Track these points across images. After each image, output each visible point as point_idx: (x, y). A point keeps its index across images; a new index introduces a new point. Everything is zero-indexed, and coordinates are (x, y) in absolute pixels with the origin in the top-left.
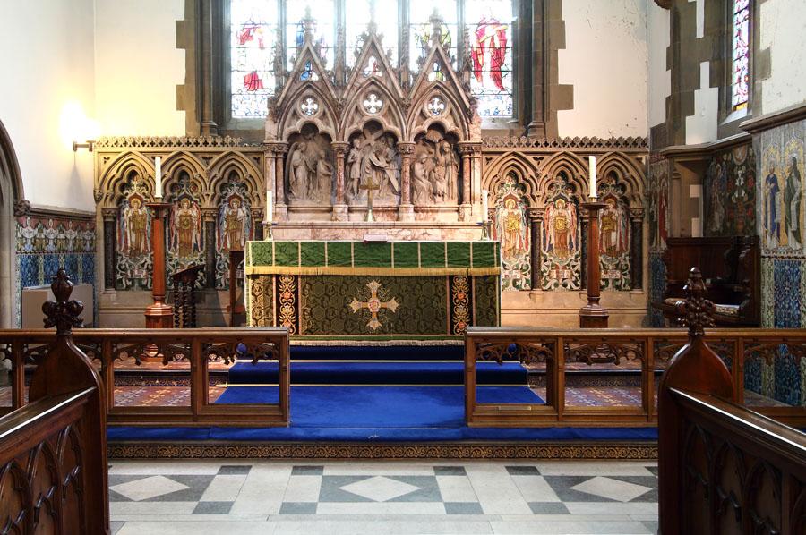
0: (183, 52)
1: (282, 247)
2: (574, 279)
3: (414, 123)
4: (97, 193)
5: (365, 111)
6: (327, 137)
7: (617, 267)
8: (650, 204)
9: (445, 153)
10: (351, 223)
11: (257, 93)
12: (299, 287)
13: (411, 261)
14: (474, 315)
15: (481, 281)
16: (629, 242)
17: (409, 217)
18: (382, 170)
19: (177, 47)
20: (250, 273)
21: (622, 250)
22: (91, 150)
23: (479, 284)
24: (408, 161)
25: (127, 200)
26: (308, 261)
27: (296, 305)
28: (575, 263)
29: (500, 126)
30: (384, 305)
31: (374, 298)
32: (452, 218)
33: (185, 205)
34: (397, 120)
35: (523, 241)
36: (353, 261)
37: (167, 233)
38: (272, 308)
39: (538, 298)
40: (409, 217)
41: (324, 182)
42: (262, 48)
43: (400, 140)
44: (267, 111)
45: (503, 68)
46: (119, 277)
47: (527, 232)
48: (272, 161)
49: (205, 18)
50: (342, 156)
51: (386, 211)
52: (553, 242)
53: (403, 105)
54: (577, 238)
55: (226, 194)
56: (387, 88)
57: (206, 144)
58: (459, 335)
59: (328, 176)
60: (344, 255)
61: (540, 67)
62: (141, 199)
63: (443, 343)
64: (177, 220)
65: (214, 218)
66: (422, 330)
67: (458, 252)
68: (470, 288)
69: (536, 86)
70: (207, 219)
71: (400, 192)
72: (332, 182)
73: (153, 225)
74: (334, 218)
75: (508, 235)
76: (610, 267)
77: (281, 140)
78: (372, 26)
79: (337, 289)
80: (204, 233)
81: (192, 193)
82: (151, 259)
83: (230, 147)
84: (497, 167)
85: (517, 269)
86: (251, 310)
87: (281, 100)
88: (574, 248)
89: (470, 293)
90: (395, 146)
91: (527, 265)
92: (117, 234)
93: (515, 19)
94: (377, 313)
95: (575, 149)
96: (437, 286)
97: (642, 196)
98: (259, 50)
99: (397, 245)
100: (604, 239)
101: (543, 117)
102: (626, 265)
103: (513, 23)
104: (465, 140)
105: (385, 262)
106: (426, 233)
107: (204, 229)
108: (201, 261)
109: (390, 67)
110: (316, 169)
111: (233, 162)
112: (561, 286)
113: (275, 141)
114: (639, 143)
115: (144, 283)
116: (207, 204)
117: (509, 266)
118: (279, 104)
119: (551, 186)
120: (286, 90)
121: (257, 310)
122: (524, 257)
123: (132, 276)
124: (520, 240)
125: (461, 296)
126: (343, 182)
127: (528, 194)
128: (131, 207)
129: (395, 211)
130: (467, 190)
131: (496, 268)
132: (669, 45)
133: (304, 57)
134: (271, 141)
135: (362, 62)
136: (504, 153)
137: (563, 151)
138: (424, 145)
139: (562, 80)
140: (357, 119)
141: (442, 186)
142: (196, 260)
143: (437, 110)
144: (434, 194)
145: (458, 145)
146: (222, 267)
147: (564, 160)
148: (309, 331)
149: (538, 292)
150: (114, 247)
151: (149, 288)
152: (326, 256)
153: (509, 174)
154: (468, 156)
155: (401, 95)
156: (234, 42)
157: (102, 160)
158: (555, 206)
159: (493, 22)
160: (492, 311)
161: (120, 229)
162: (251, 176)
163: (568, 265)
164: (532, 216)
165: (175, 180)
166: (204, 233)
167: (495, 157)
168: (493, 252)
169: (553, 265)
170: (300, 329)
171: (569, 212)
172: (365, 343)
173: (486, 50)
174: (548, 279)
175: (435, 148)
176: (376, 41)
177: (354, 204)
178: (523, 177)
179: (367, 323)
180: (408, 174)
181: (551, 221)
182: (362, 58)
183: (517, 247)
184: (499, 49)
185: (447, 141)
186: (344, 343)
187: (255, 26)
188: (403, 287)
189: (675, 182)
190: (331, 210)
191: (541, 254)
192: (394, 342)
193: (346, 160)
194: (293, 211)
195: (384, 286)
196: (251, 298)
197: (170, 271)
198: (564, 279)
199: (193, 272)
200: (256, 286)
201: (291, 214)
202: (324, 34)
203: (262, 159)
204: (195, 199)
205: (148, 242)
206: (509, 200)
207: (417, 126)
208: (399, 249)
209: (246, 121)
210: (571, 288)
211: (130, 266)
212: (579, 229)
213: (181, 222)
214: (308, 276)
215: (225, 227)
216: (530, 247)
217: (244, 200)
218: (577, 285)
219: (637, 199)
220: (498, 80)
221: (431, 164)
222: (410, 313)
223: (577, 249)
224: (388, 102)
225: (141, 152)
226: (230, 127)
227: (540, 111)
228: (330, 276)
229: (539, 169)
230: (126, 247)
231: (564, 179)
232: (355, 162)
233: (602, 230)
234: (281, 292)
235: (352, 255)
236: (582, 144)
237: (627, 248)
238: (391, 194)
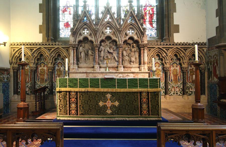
0: (41, 14)
1: (71, 80)
2: (180, 91)
3: (123, 37)
4: (10, 62)
5: (105, 33)
6: (92, 42)
9: (134, 47)
10: (100, 72)
11: (68, 29)
12: (78, 96)
13: (124, 86)
14: (150, 108)
15: (153, 94)
17: (121, 70)
18: (112, 53)
19: (39, 12)
20: (58, 91)
22: (5, 46)
23: (152, 95)
24: (121, 50)
26: (82, 86)
27: (77, 104)
28: (180, 86)
29: (152, 39)
30: (113, 104)
31: (109, 101)
32: (137, 70)
33: (42, 66)
34: (117, 36)
36: (100, 86)
38: (67, 105)
39: (168, 98)
40: (122, 70)
41: (91, 58)
42: (70, 14)
43: (118, 43)
44: (70, 33)
45: (153, 20)
46: (19, 90)
48: (72, 50)
49: (50, 3)
50: (97, 48)
51: (113, 68)
52: (172, 78)
53: (119, 31)
54: (181, 77)
55: (57, 62)
56: (113, 25)
57: (49, 45)
58: (144, 116)
59: (92, 55)
60: (97, 83)
61: (167, 19)
63: (137, 119)
64: (40, 71)
65: (52, 70)
66: (129, 114)
67: (143, 82)
68: (148, 97)
69: (166, 25)
70: (50, 71)
71: (118, 61)
72: (94, 58)
73: (31, 73)
74: (94, 70)
77: (75, 43)
78: (108, 4)
79: (94, 97)
80: (49, 75)
81: (45, 62)
82: (30, 84)
83: (58, 46)
84: (153, 52)
86: (58, 105)
87: (75, 29)
88: (180, 81)
89: (148, 99)
90: (116, 45)
91: (163, 87)
92: (18, 76)
93: (157, 4)
94: (110, 107)
95: (180, 46)
96: (135, 96)
97: (205, 63)
98: (69, 15)
99: (118, 79)
101: (168, 36)
103: (156, 6)
104: (141, 43)
105: (113, 86)
106: (128, 75)
107: (49, 74)
108: (48, 85)
109: (114, 18)
110: (88, 53)
111: (59, 51)
112: (175, 94)
113: (73, 43)
114: (203, 44)
115: (28, 92)
116: (50, 65)
118: (74, 30)
119: (171, 60)
120: (77, 25)
121: (61, 106)
125: (145, 100)
126: (97, 58)
127: (164, 62)
129: (116, 68)
130: (142, 60)
131: (159, 89)
132: (217, 8)
133: (84, 14)
134: (72, 43)
135: (105, 17)
136: (155, 47)
137: (176, 47)
138: (127, 45)
139: (175, 23)
140: (103, 36)
141: (133, 59)
142: (46, 85)
143: (131, 33)
144: (130, 62)
145: (139, 45)
148: (82, 114)
149: (167, 96)
151: (30, 94)
152: (89, 84)
153: (157, 55)
154: (142, 48)
155: (118, 27)
156: (61, 12)
157: (13, 50)
158: (173, 66)
159: (149, 5)
160: (157, 106)
161: (19, 74)
162: (65, 56)
163: (178, 86)
164: (165, 69)
165: (39, 57)
166: (49, 75)
167: (152, 49)
168: (157, 82)
170: (78, 113)
171: (178, 68)
172: (105, 119)
173: (147, 15)
174: (171, 91)
175: (130, 46)
176: (109, 9)
177: (101, 65)
178: (162, 56)
179: (106, 111)
180: (121, 55)
181: (172, 71)
182: (104, 15)
184: (152, 14)
185: (135, 44)
186: (96, 119)
187: (68, 7)
188: (121, 96)
189: (221, 57)
190: (93, 67)
191: (168, 83)
192: (117, 119)
193: (99, 50)
194: (80, 68)
195: (113, 96)
196: (59, 100)
198: (176, 92)
199: (44, 89)
200: (61, 96)
201: (79, 69)
202: (92, 9)
203: (69, 50)
204: (46, 64)
205: (29, 79)
206: (157, 64)
207: (124, 38)
208: (119, 81)
209: (65, 38)
210: (179, 94)
212: (182, 74)
213: (41, 72)
214: (81, 92)
215: (56, 73)
216: (164, 80)
217: (63, 64)
218: (181, 94)
220: (151, 24)
221: (129, 51)
222: (124, 107)
223: (181, 81)
224: (114, 30)
225: (26, 48)
226: (59, 40)
227: (167, 34)
228: (91, 92)
229: (168, 53)
231: (176, 57)
232: (102, 51)
233: (190, 74)
234: (71, 98)
235: (100, 83)
236: (183, 45)
238: (115, 62)
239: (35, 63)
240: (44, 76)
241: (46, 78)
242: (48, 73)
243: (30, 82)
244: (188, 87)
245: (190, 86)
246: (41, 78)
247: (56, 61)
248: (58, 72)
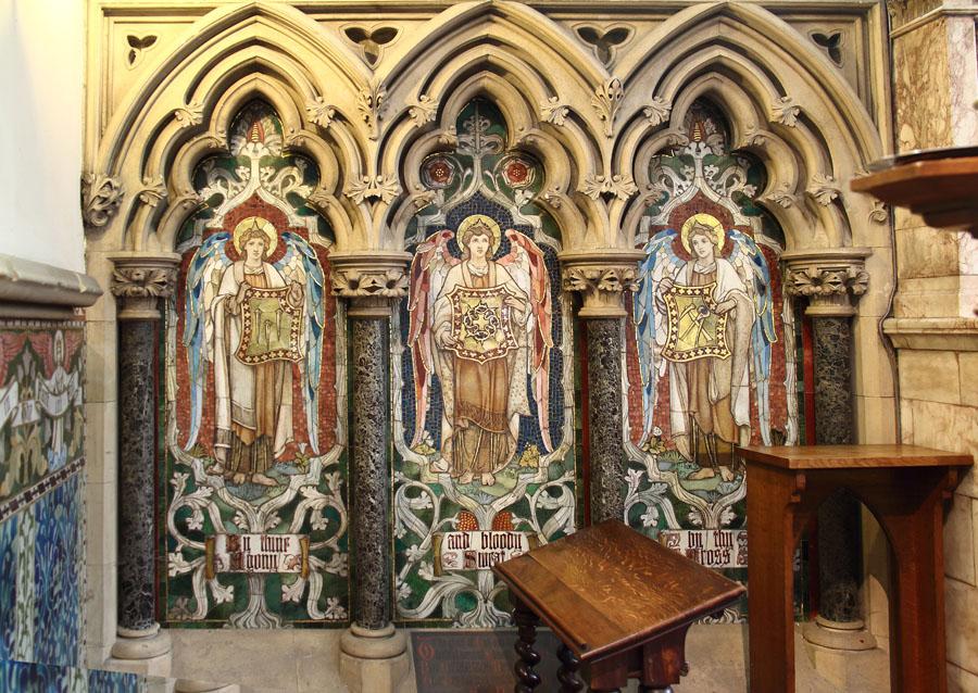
4: (95, 191)
25: (216, 222)
28: (548, 503)
33: (479, 245)
37: (397, 370)
46: (177, 565)
62: (277, 217)
64: (443, 311)
81: (509, 193)
82: (322, 487)
92: (171, 374)
107: (567, 348)
108: (554, 492)
111: (256, 52)
115: (292, 592)
123: (237, 559)
128: (233, 255)
142: (532, 488)
146: (195, 523)
150: (158, 433)
161: (181, 354)
163: (520, 507)
174: (427, 573)
197: (411, 538)
205: (311, 410)
206: (248, 223)
211: (228, 515)
215: (661, 339)
230: (209, 430)
239: (406, 211)
240: (508, 375)
241: (533, 405)
242: (549, 343)
243: (324, 451)
244: (195, 523)
245: (676, 503)
246: (460, 408)
247: (205, 184)
248: (685, 323)
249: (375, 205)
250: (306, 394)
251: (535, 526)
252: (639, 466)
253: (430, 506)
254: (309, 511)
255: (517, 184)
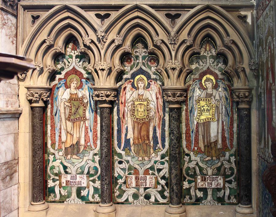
2: (160, 188)
7: (219, 171)
8: (258, 82)
16: (235, 136)
21: (225, 147)
28: (161, 167)
33: (73, 85)
35: (90, 134)
47: (96, 121)
52: (130, 136)
54: (163, 131)
75: (69, 124)
76: (210, 172)
85: (82, 173)
88: (160, 145)
97: (248, 70)
100: (200, 133)
102: (231, 169)
112: (142, 198)
117: (72, 170)
122: (91, 157)
124: (86, 133)
142: (156, 162)
147: (68, 18)
158: (133, 85)
163: (152, 168)
169: (130, 168)
174: (124, 188)
183: (82, 142)
198: (146, 189)
210: (156, 200)
218: (164, 197)
219: (242, 75)
223: (164, 146)
237: (232, 145)
245: (200, 167)
249: (175, 71)
250: (89, 130)
251: (156, 173)
252: (188, 155)
253: (125, 167)
254: (89, 168)
255: (152, 65)
